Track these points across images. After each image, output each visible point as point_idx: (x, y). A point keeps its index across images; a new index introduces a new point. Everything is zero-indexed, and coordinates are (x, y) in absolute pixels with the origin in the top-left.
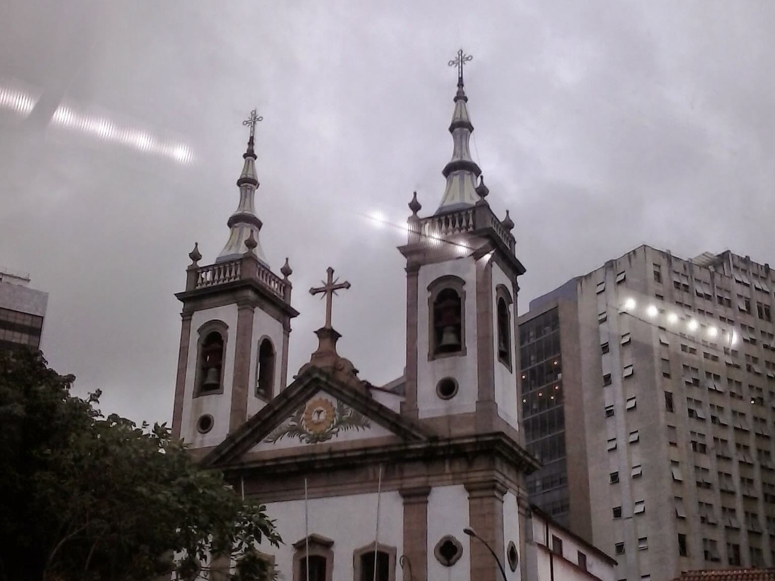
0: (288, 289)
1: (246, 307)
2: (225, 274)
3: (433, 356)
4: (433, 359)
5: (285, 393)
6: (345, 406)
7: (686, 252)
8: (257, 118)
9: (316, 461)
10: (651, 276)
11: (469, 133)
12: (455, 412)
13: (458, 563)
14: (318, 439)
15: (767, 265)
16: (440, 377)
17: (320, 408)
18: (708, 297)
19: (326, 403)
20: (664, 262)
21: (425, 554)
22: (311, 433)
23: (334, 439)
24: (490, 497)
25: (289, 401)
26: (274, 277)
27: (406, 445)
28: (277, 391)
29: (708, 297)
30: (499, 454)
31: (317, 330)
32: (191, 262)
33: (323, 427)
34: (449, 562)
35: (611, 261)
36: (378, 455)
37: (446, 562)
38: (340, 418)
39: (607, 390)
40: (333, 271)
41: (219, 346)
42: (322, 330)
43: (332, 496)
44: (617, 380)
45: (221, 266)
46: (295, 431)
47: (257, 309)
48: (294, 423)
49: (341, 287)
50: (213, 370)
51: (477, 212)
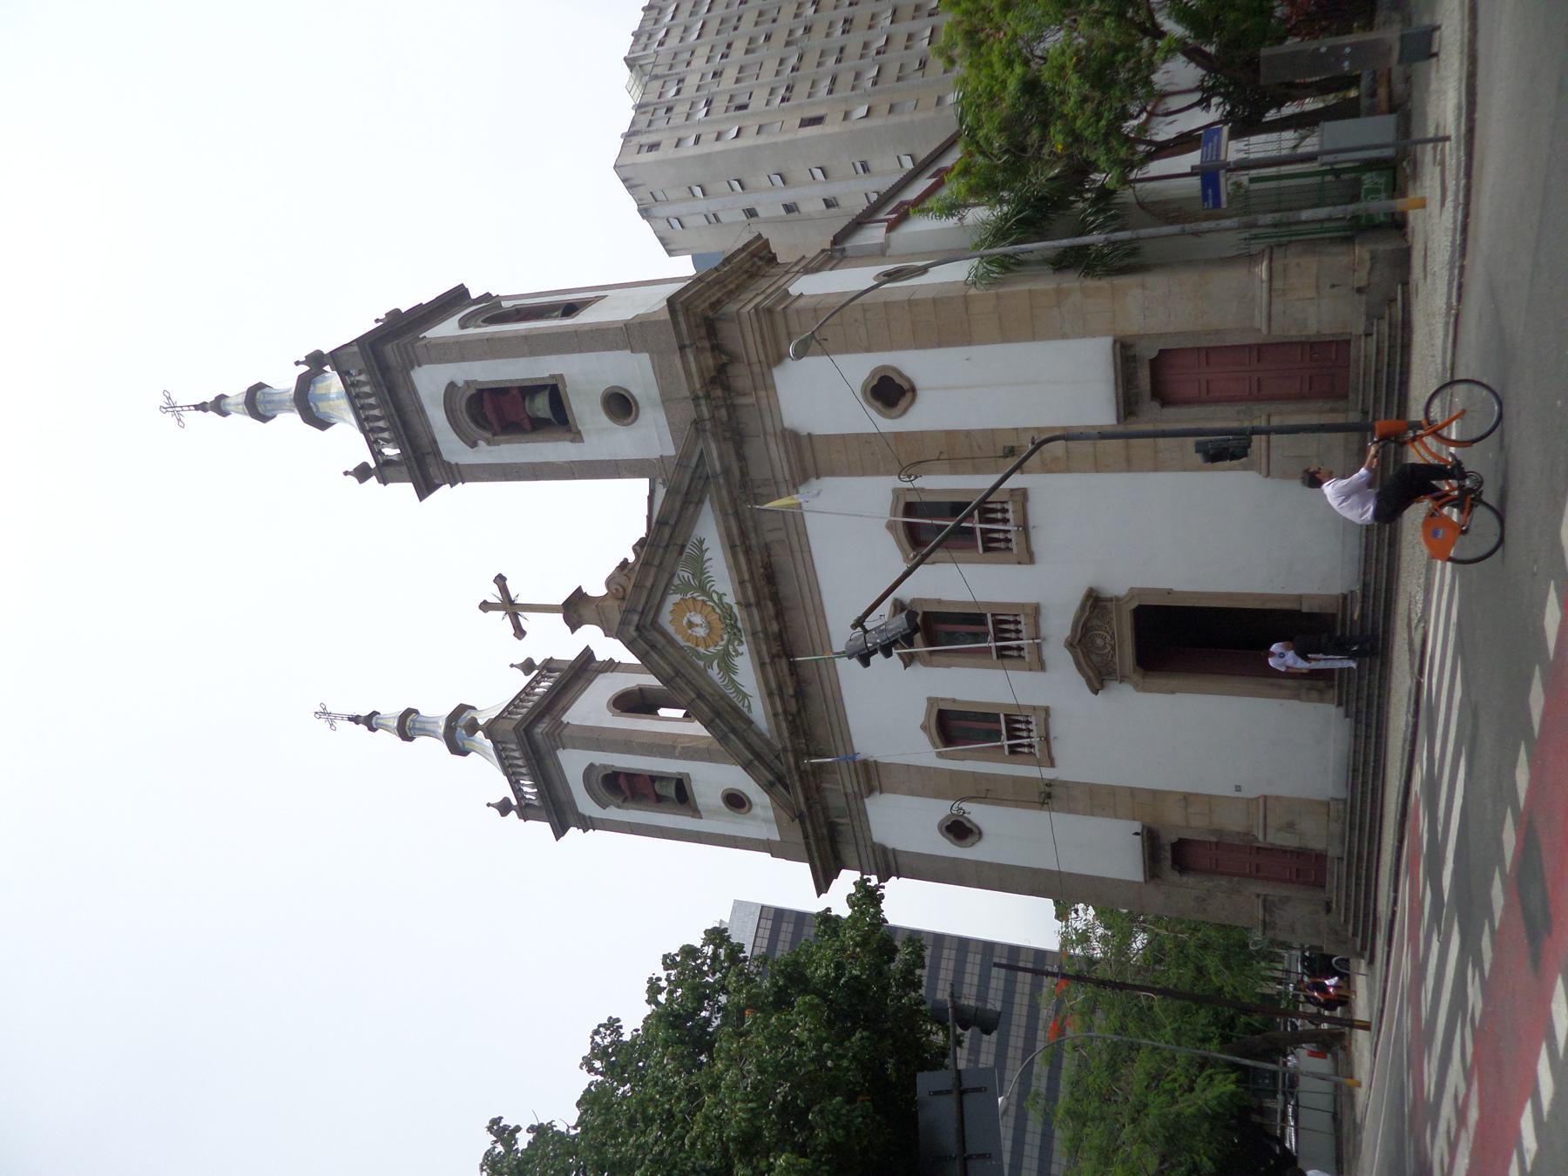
0: (552, 666)
3: (577, 437)
4: (579, 432)
6: (676, 581)
7: (624, 116)
9: (765, 630)
10: (652, 156)
11: (267, 390)
12: (655, 392)
13: (908, 372)
14: (734, 626)
15: (644, 9)
19: (679, 609)
20: (636, 140)
21: (898, 436)
22: (726, 637)
24: (785, 316)
25: (678, 673)
26: (530, 687)
27: (715, 476)
30: (715, 305)
31: (568, 629)
32: (513, 814)
33: (714, 617)
34: (908, 391)
35: (639, 210)
37: (909, 395)
39: (803, 208)
40: (485, 602)
43: (821, 603)
44: (789, 196)
46: (727, 668)
47: (565, 719)
48: (715, 664)
49: (504, 589)
50: (657, 786)
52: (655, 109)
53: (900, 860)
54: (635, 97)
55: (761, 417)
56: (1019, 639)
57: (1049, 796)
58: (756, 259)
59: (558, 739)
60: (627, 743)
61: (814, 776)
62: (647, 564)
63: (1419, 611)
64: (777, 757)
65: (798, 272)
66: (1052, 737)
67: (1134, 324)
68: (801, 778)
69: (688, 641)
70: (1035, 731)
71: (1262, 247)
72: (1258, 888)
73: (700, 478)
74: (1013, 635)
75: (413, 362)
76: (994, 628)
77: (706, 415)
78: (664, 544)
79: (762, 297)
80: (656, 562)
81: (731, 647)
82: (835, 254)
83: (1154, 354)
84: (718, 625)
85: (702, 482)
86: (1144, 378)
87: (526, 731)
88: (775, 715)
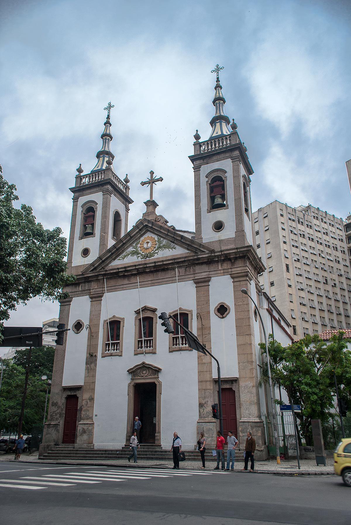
0: (127, 189)
1: (107, 193)
2: (95, 178)
4: (210, 212)
5: (129, 234)
6: (162, 239)
8: (111, 106)
9: (147, 267)
12: (223, 238)
14: (147, 257)
17: (149, 241)
19: (152, 239)
22: (143, 254)
23: (156, 256)
25: (131, 237)
28: (123, 234)
30: (249, 259)
34: (223, 316)
36: (182, 262)
37: (221, 316)
38: (159, 245)
40: (153, 173)
41: (93, 214)
42: (148, 201)
45: (94, 173)
46: (133, 253)
47: (112, 195)
52: (294, 215)
53: (67, 306)
54: (298, 208)
55: (215, 271)
56: (145, 347)
57: (92, 356)
58: (260, 268)
59: (106, 193)
60: (105, 216)
61: (96, 280)
62: (168, 231)
63: (170, 467)
64: (103, 268)
65: (256, 282)
66: (112, 357)
67: (242, 383)
68: (96, 275)
69: (142, 241)
70: (114, 352)
71: (263, 420)
72: (62, 422)
73: (196, 250)
74: (146, 345)
75: (233, 159)
76: (148, 339)
77: (216, 254)
78: (175, 237)
79: (250, 272)
80: (169, 234)
81: (140, 255)
82: (260, 291)
83: (233, 389)
84: (147, 252)
85: (195, 251)
86: (227, 386)
87: (109, 182)
88: (118, 269)
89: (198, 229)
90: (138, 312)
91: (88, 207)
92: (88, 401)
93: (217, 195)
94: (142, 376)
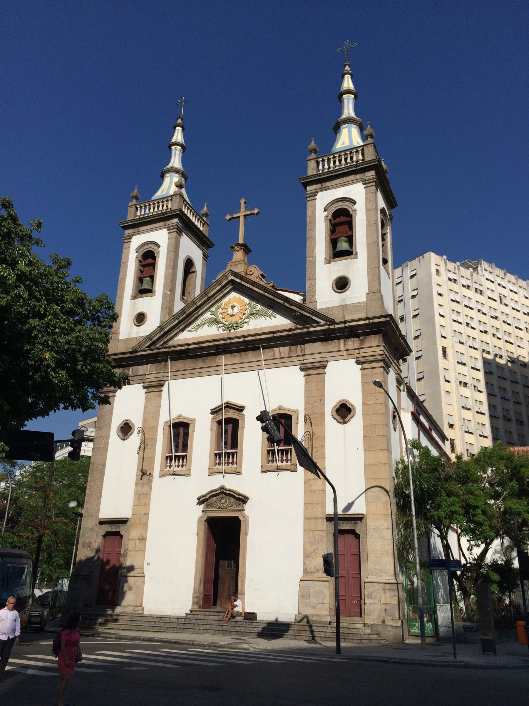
4: (329, 263)
10: (434, 272)
12: (348, 302)
16: (336, 276)
17: (235, 304)
18: (468, 287)
21: (323, 414)
22: (227, 323)
23: (246, 327)
29: (468, 287)
34: (344, 421)
37: (342, 421)
41: (153, 261)
46: (215, 321)
51: (365, 149)
59: (173, 230)
89: (310, 287)
90: (215, 411)
91: (145, 251)
92: (137, 541)
93: (341, 237)
94: (220, 508)
